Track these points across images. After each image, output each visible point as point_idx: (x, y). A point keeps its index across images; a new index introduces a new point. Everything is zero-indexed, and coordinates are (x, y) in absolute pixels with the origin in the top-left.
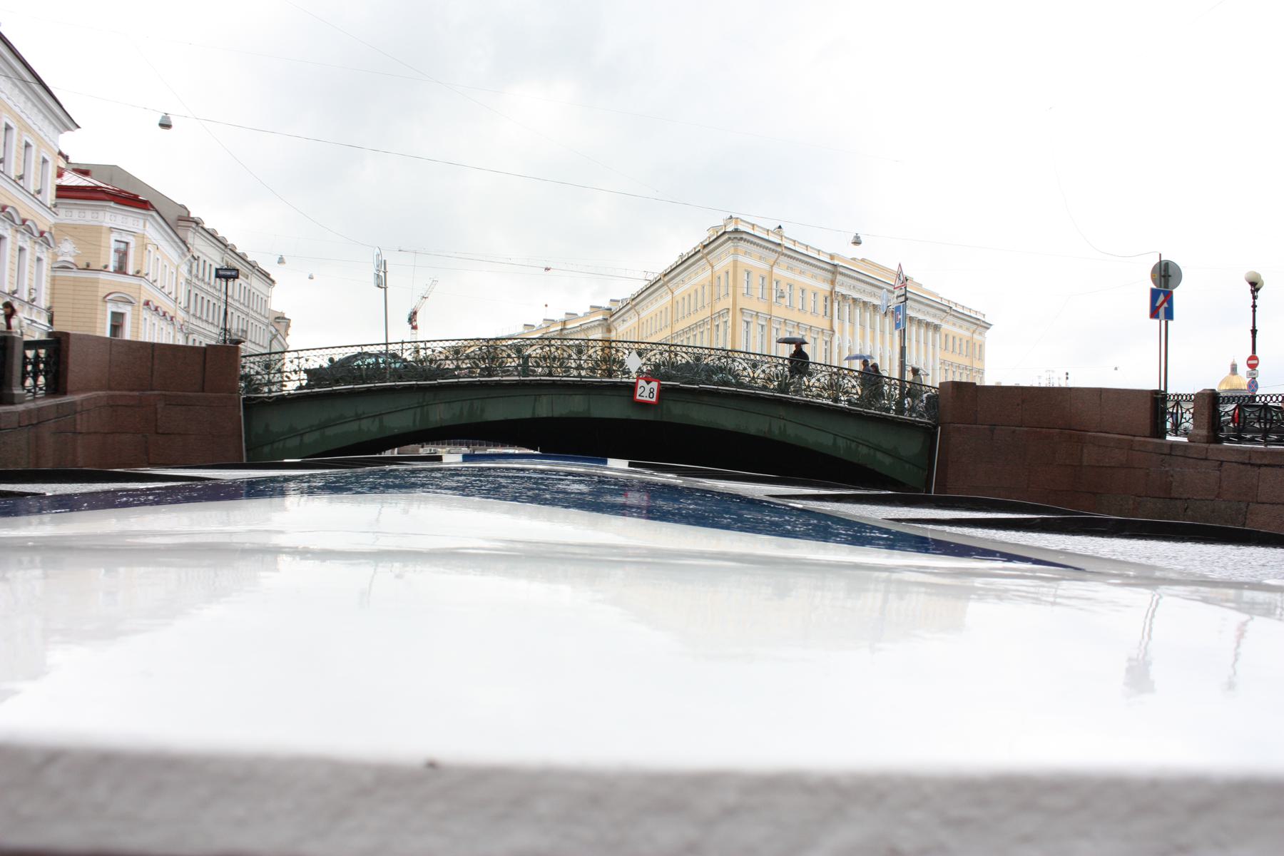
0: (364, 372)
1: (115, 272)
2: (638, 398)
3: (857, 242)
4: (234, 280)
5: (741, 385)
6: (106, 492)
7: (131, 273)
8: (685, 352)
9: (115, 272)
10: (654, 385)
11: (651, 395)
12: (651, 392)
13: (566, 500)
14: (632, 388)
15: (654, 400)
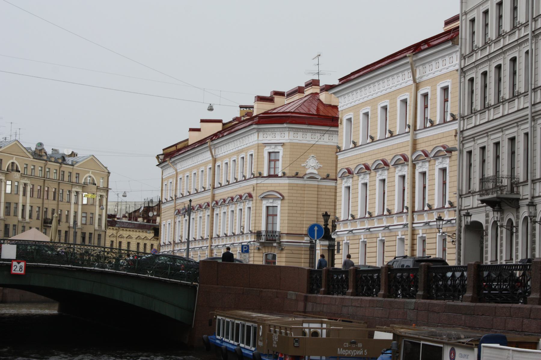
0: (69, 259)
2: (13, 272)
3: (211, 109)
4: (268, 248)
10: (23, 264)
11: (21, 270)
12: (20, 268)
13: (313, 254)
14: (10, 266)
15: (23, 272)
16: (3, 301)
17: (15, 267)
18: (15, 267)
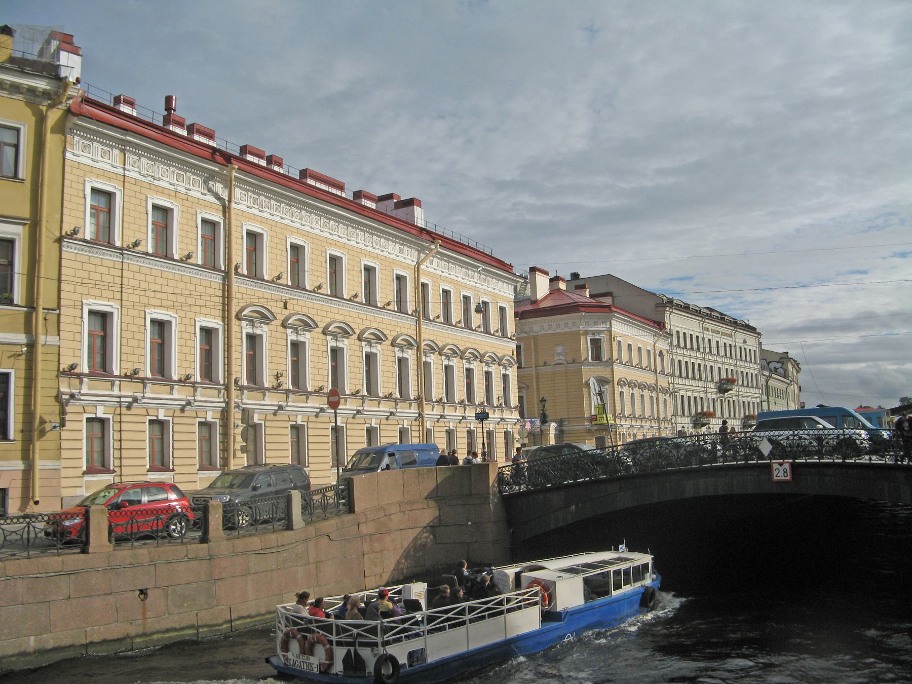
1: (91, 375)
2: (775, 478)
5: (670, 464)
6: (397, 638)
7: (176, 257)
8: (758, 437)
9: (91, 375)
11: (786, 475)
12: (785, 472)
15: (788, 478)
16: (5, 458)
17: (777, 471)
18: (777, 471)
